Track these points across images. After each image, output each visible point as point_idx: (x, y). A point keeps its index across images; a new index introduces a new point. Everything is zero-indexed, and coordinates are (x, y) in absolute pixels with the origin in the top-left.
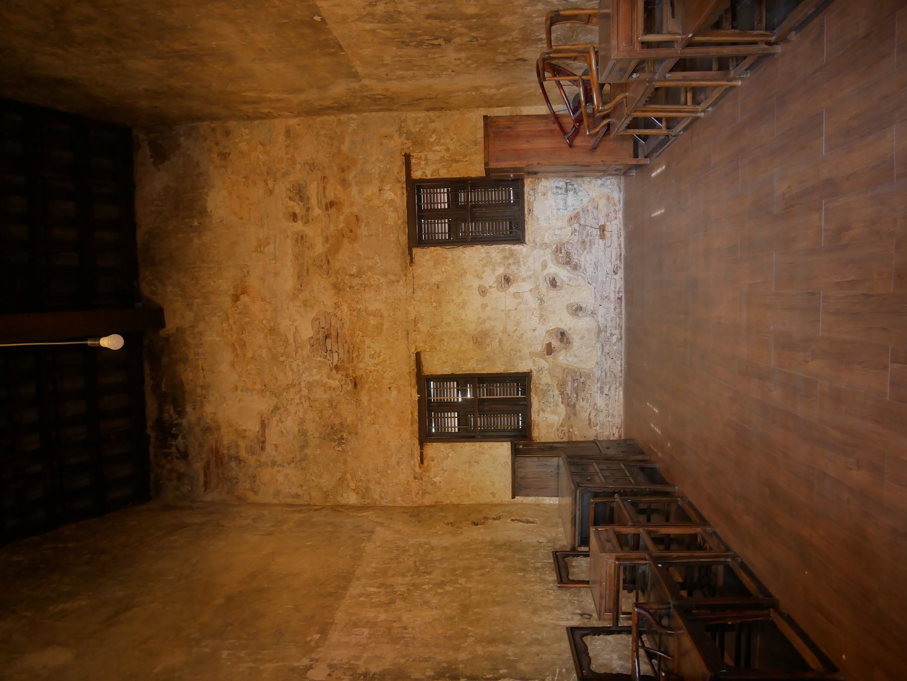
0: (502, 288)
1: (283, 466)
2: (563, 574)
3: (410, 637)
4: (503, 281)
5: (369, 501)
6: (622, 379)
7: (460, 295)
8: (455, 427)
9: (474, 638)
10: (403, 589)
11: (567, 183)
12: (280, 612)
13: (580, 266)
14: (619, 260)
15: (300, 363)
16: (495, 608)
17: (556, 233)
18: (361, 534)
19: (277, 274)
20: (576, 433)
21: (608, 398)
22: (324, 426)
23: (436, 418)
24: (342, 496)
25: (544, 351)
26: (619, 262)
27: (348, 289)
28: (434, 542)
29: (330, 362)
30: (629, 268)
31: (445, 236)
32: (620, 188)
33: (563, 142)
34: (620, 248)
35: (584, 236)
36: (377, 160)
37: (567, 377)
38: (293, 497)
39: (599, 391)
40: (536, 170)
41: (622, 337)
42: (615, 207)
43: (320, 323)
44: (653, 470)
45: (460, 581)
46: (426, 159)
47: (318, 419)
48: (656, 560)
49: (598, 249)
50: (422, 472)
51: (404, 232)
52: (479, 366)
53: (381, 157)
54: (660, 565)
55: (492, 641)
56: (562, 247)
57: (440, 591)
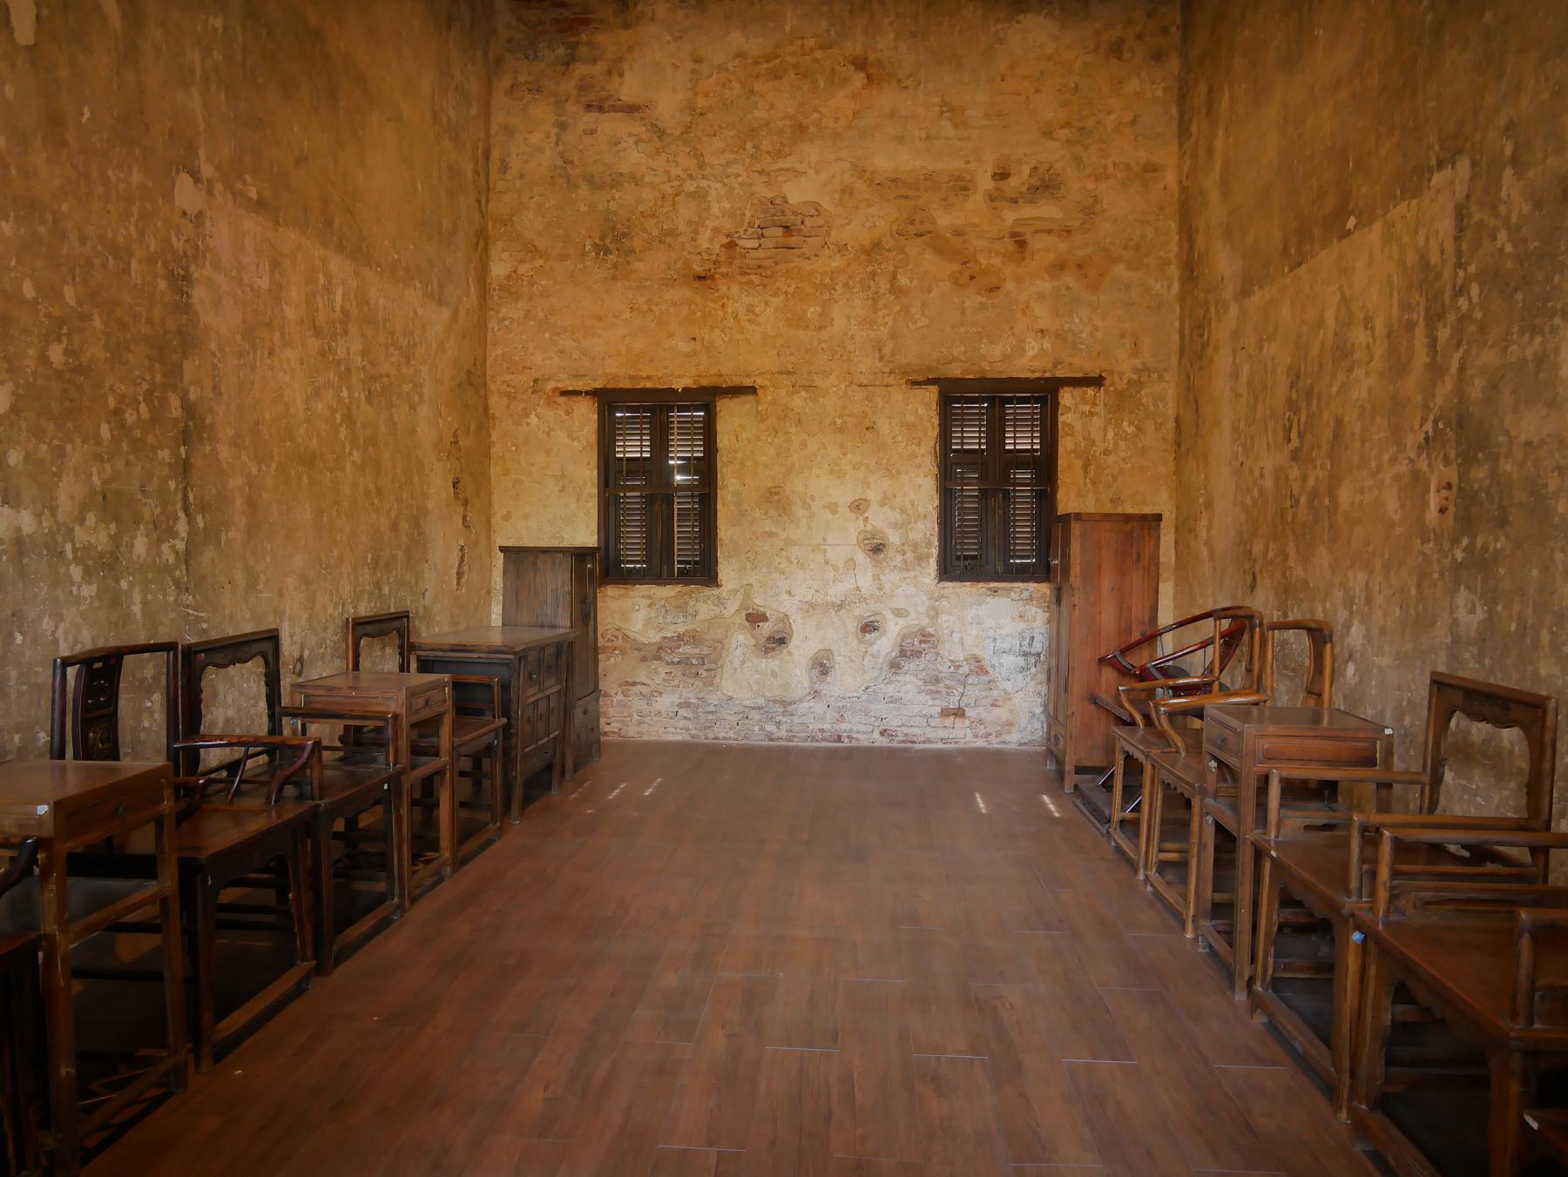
2: (369, 628)
3: (255, 361)
5: (496, 298)
6: (702, 740)
7: (854, 466)
8: (624, 452)
10: (341, 351)
11: (1039, 655)
12: (295, 129)
15: (740, 179)
19: (901, 140)
20: (612, 660)
21: (671, 715)
24: (504, 250)
26: (901, 738)
27: (870, 268)
28: (424, 411)
29: (742, 233)
30: (891, 753)
31: (956, 444)
32: (1024, 744)
33: (1108, 648)
34: (924, 742)
36: (1096, 328)
38: (503, 161)
39: (682, 701)
40: (1064, 603)
43: (812, 216)
44: (549, 786)
46: (1092, 414)
47: (640, 209)
48: (395, 780)
53: (1099, 335)
54: (386, 787)
55: (251, 504)
57: (338, 417)
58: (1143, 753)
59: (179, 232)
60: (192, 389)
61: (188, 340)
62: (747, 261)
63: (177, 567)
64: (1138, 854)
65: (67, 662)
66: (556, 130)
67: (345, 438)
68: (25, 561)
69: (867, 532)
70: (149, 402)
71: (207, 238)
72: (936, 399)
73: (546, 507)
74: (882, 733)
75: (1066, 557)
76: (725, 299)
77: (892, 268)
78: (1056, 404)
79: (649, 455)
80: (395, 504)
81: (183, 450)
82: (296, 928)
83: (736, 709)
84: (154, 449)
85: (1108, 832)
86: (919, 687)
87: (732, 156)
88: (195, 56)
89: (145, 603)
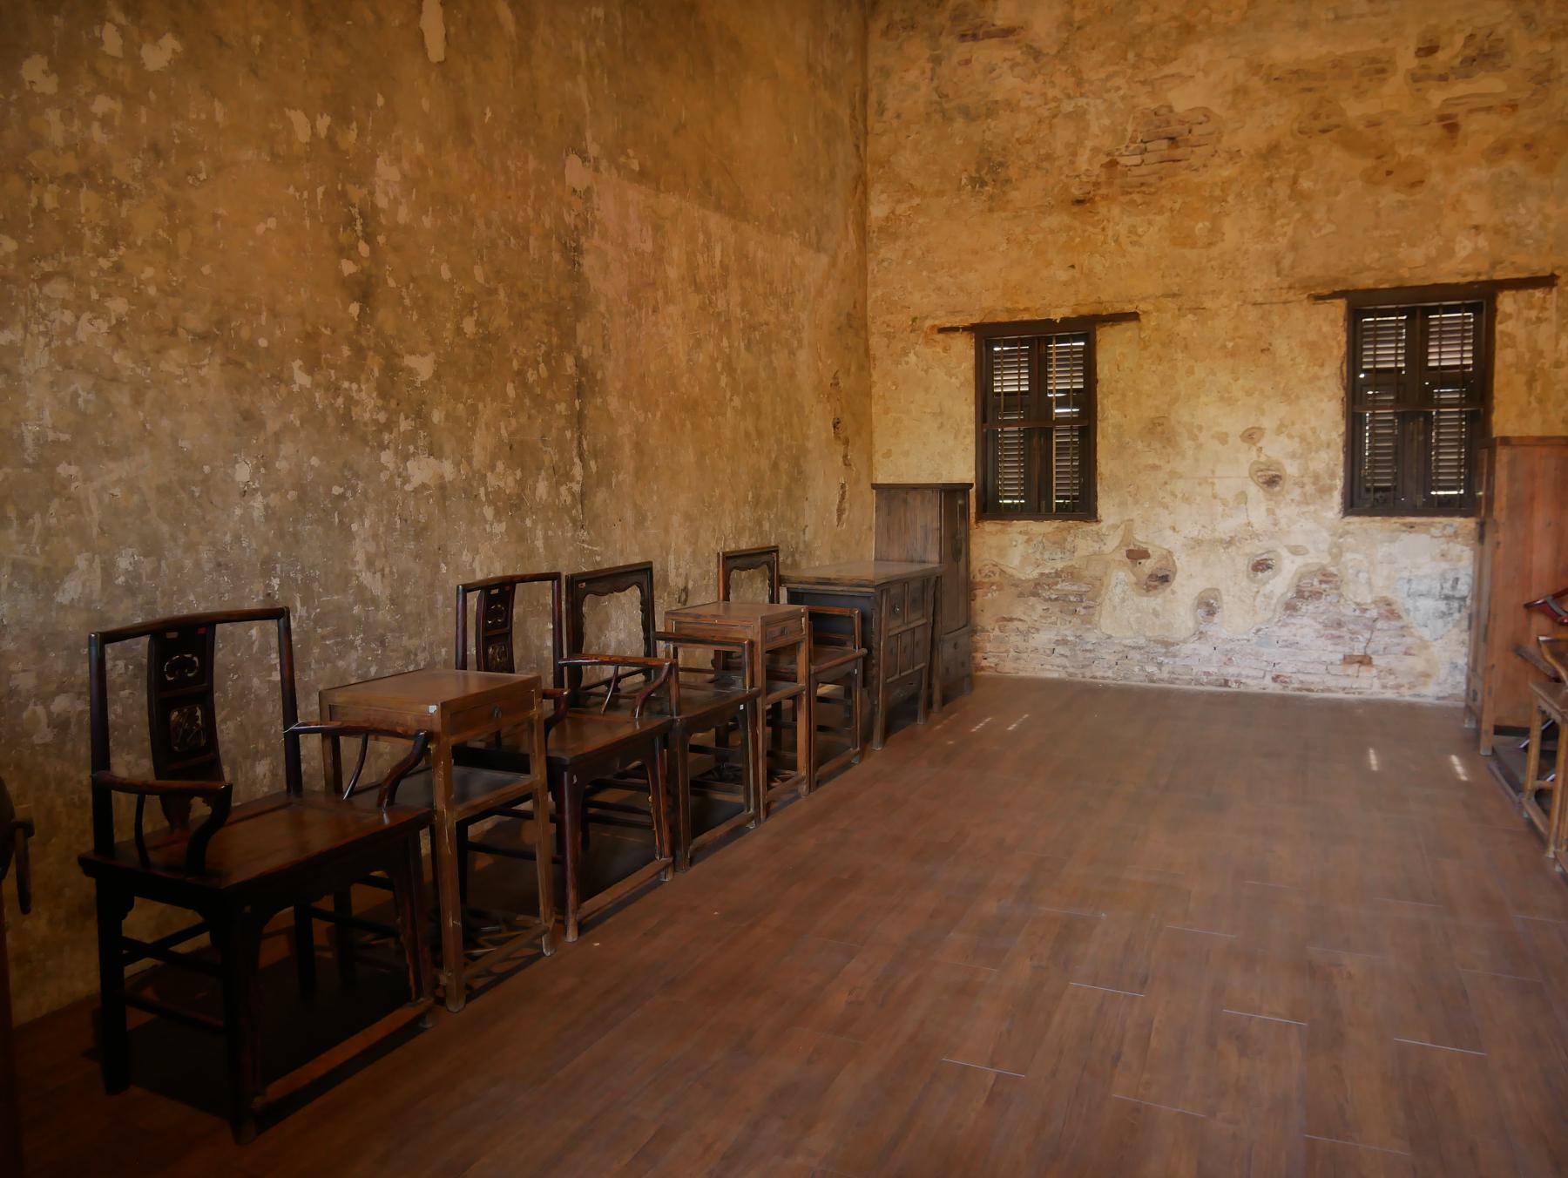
0: (1257, 471)
1: (932, 79)
2: (739, 562)
3: (641, 319)
4: (1270, 473)
5: (875, 240)
6: (1079, 678)
7: (1247, 392)
8: (1002, 387)
9: (643, 420)
10: (721, 304)
11: (1463, 599)
12: (674, 100)
13: (1292, 616)
14: (1300, 686)
15: (1121, 93)
16: (692, 456)
17: (1361, 575)
18: (814, 228)
19: (1304, 25)
20: (989, 595)
21: (1048, 652)
22: (1004, 149)
23: (1019, 354)
24: (882, 192)
25: (1134, 545)
26: (1296, 685)
27: (1267, 174)
28: (803, 355)
29: (1123, 151)
30: (1281, 702)
31: (1367, 363)
32: (1443, 698)
33: (1538, 594)
34: (1322, 691)
35: (1351, 627)
36: (1547, 218)
37: (1086, 584)
38: (880, 103)
39: (1059, 638)
40: (1487, 539)
41: (1154, 682)
42: (1407, 686)
43: (1201, 123)
44: (913, 716)
45: (735, 398)
46: (1539, 320)
47: (1017, 135)
48: (751, 700)
49: (1324, 650)
50: (923, 331)
51: (1381, 280)
52: (1110, 429)
53: (1552, 226)
54: (742, 707)
55: (638, 447)
56: (1332, 585)
57: (719, 366)
58: (1559, 713)
59: (570, 208)
60: (584, 348)
61: (580, 304)
62: (1128, 179)
63: (573, 507)
64: (1548, 827)
65: (467, 589)
66: (930, 65)
67: (726, 385)
68: (447, 503)
69: (1261, 463)
70: (547, 361)
71: (595, 211)
72: (1343, 314)
73: (924, 444)
74: (1275, 679)
75: (1490, 487)
76: (1105, 223)
77: (1292, 172)
78: (1493, 311)
79: (1027, 389)
80: (775, 446)
81: (577, 403)
82: (655, 826)
83: (1115, 649)
84: (552, 403)
85: (1520, 803)
86: (1316, 631)
87: (1111, 69)
88: (579, 47)
89: (546, 538)
